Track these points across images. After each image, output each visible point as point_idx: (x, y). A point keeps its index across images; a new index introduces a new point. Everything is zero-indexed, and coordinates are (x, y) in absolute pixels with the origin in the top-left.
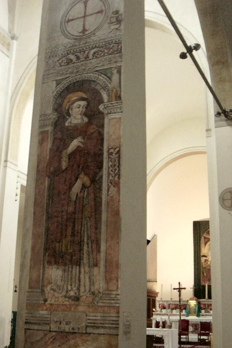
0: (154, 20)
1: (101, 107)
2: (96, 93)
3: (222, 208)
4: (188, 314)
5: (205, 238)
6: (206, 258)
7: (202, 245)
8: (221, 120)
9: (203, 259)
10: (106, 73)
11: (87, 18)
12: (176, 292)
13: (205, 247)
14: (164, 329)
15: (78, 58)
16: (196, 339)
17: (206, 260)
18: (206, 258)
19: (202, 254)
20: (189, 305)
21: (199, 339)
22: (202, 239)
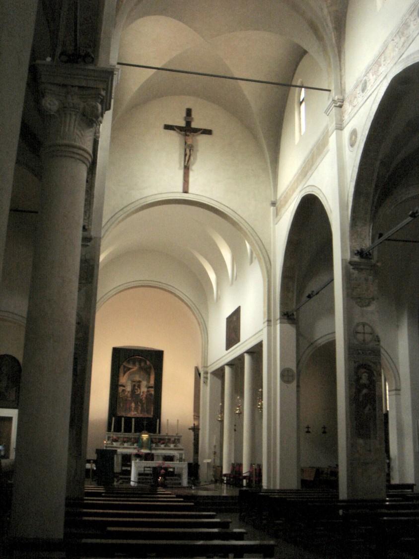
0: (231, 216)
1: (374, 378)
2: (373, 373)
3: (283, 383)
4: (141, 447)
5: (125, 367)
6: (124, 388)
7: (121, 374)
8: (284, 319)
9: (121, 389)
10: (375, 363)
11: (366, 332)
12: (192, 433)
13: (123, 376)
14: (181, 463)
15: (363, 353)
16: (402, 474)
17: (123, 390)
18: (124, 388)
19: (120, 383)
20: (142, 439)
21: (122, 470)
22: (122, 367)
